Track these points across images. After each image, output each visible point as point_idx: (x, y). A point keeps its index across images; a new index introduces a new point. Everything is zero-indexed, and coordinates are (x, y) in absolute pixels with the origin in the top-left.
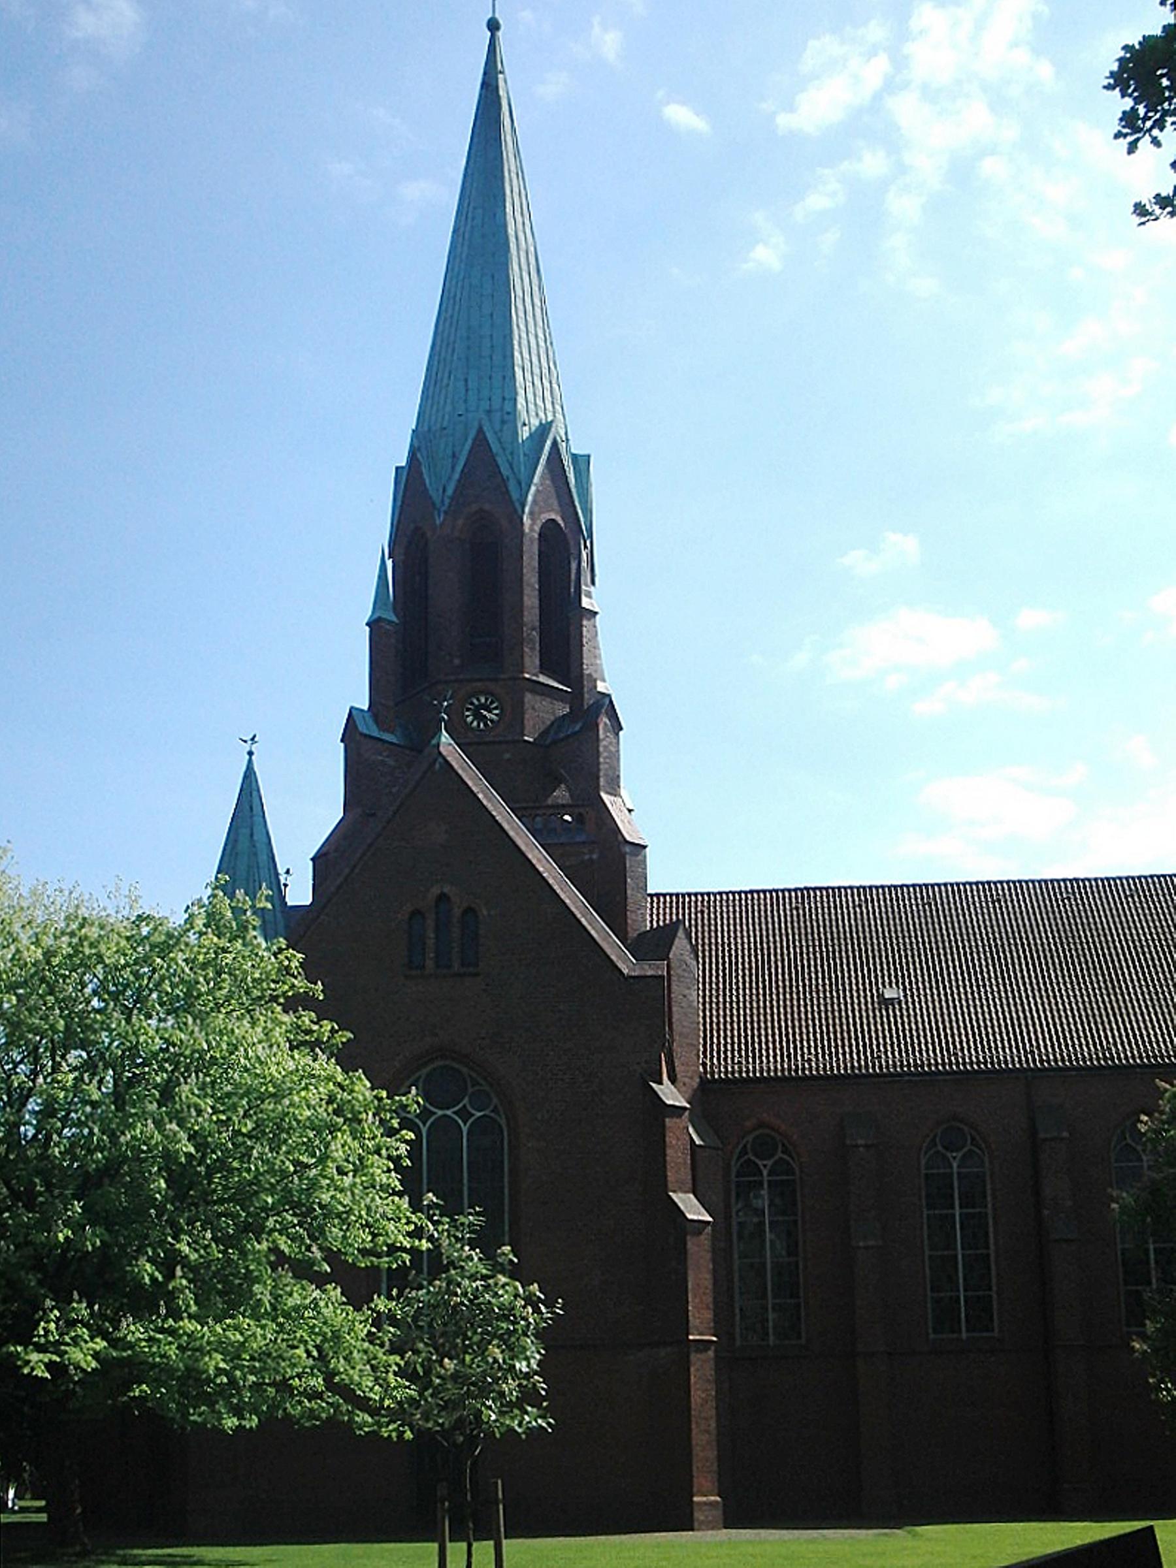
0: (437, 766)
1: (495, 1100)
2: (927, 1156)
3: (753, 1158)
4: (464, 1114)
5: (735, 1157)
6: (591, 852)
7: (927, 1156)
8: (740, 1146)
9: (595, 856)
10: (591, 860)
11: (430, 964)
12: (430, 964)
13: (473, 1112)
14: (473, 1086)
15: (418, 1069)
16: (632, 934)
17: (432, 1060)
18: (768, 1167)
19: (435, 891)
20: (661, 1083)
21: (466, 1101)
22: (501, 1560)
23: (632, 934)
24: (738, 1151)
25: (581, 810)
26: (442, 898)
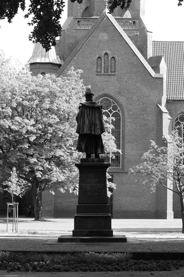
0: (105, 19)
1: (119, 108)
2: (112, 102)
3: (179, 121)
4: (119, 111)
5: (175, 121)
6: (137, 33)
7: (112, 102)
8: (176, 118)
9: (138, 34)
10: (137, 35)
11: (103, 71)
12: (103, 71)
13: (113, 111)
14: (113, 104)
15: (99, 99)
16: (148, 57)
17: (102, 97)
18: (183, 124)
19: (104, 52)
20: (161, 105)
21: (111, 108)
22: (123, 229)
23: (148, 57)
24: (176, 119)
25: (135, 20)
26: (106, 54)
